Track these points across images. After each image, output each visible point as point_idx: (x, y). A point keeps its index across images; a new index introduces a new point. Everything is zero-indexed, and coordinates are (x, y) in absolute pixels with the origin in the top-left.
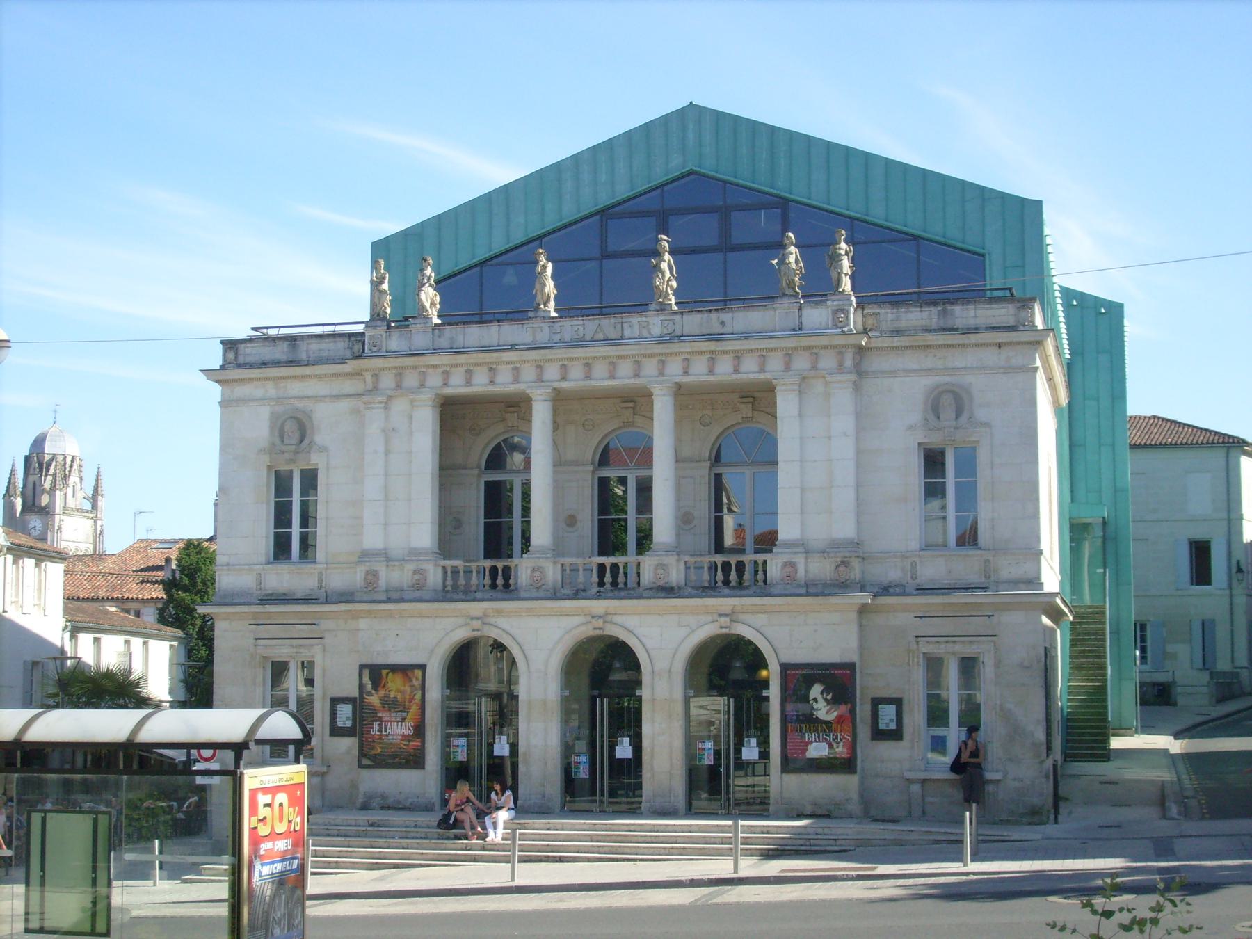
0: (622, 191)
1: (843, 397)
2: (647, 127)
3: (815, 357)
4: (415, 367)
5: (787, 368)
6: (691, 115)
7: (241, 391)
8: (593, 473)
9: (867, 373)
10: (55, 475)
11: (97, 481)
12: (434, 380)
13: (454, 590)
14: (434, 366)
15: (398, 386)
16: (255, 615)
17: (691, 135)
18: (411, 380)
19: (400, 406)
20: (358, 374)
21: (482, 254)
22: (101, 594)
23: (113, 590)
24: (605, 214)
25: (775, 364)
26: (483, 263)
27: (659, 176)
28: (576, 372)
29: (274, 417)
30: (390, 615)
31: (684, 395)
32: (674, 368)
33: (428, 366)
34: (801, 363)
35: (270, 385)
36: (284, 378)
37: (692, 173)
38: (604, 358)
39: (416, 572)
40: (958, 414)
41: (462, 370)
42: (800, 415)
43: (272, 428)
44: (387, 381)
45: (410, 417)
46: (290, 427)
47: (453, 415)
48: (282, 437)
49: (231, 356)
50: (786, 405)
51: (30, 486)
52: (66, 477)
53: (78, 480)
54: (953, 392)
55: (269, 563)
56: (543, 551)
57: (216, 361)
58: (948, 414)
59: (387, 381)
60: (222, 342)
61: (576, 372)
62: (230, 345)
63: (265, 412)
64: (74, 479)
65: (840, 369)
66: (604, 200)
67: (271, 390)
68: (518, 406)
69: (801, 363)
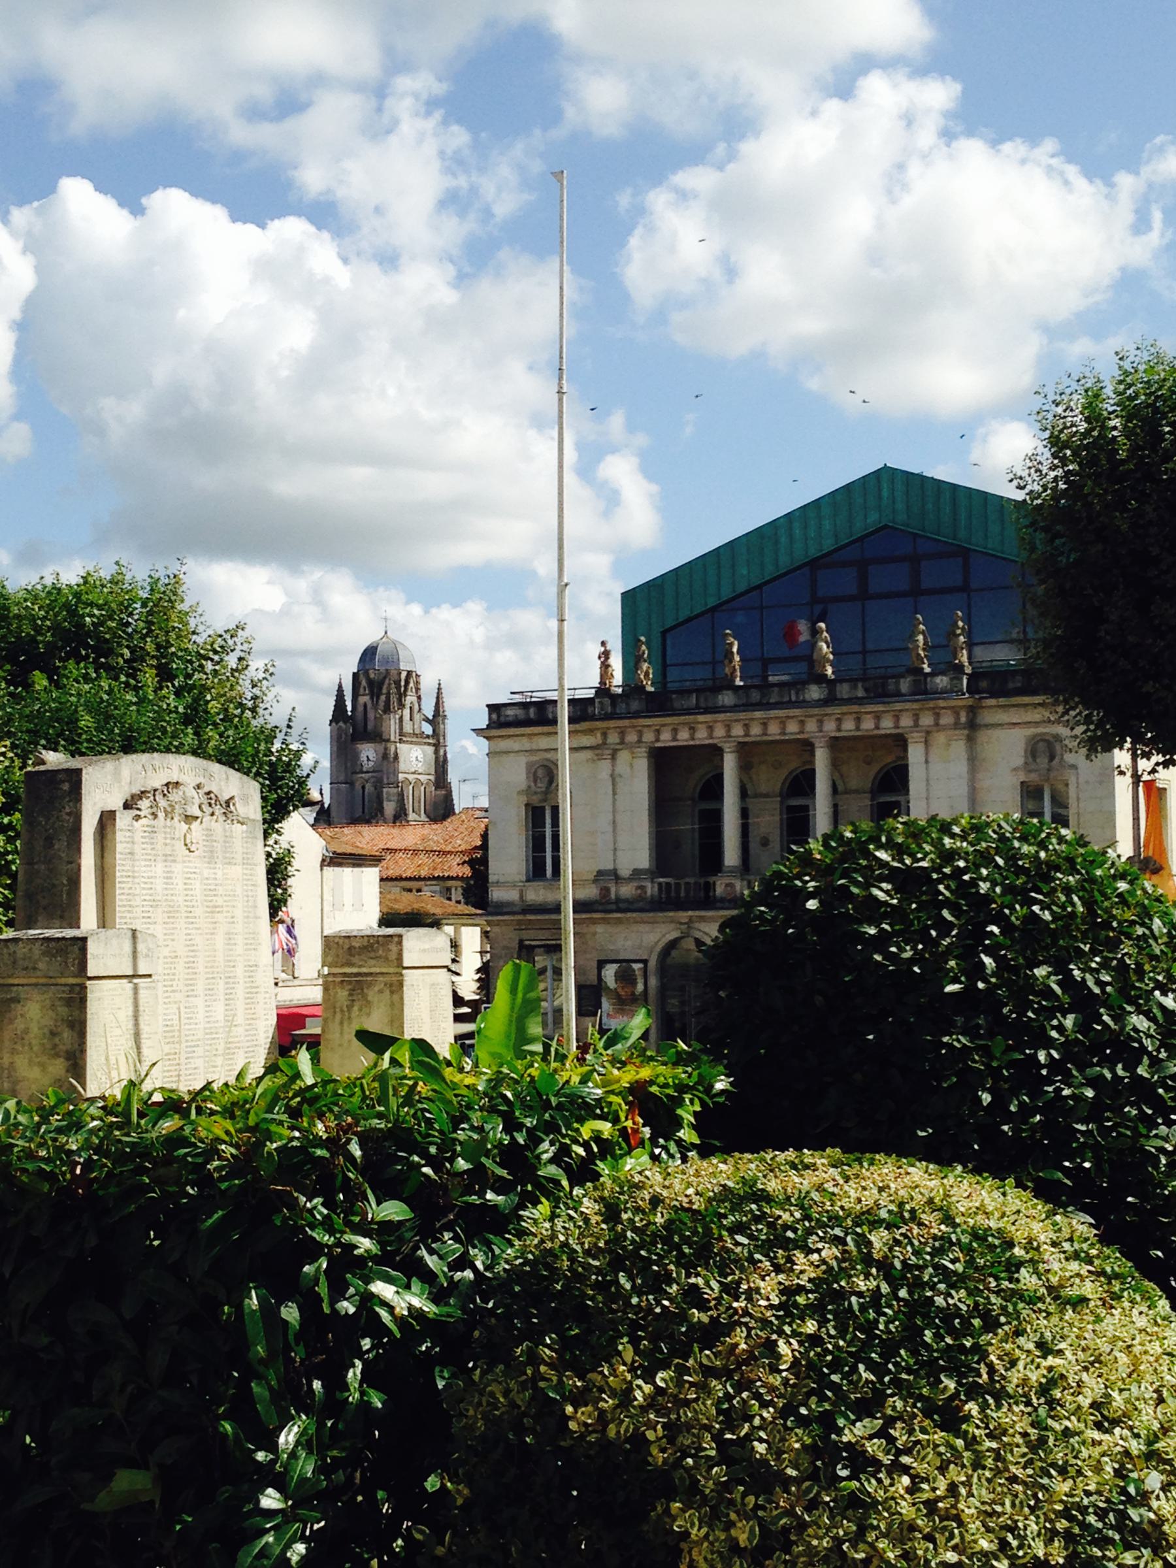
0: (828, 544)
1: (959, 748)
2: (848, 488)
3: (937, 716)
4: (634, 727)
5: (916, 725)
6: (885, 476)
7: (504, 744)
8: (782, 803)
9: (980, 726)
10: (388, 694)
11: (438, 698)
12: (649, 737)
13: (666, 902)
14: (649, 726)
15: (622, 742)
16: (519, 922)
17: (885, 493)
18: (632, 737)
19: (624, 756)
20: (591, 731)
21: (712, 602)
22: (423, 874)
23: (435, 869)
24: (814, 564)
25: (906, 721)
26: (713, 609)
27: (859, 529)
28: (756, 730)
29: (529, 765)
30: (619, 921)
31: (836, 744)
32: (830, 726)
33: (644, 726)
34: (927, 720)
35: (525, 740)
36: (536, 735)
37: (886, 527)
38: (776, 718)
39: (638, 888)
40: (1052, 758)
41: (670, 728)
42: (927, 762)
43: (528, 773)
44: (613, 738)
45: (631, 766)
46: (540, 773)
47: (664, 763)
48: (535, 781)
49: (494, 716)
50: (915, 754)
51: (360, 709)
52: (401, 696)
53: (415, 699)
54: (1042, 740)
55: (528, 880)
56: (732, 870)
57: (484, 723)
58: (1043, 761)
59: (613, 738)
60: (488, 706)
61: (756, 730)
62: (493, 708)
63: (523, 760)
64: (410, 699)
65: (956, 725)
66: (813, 552)
67: (525, 744)
68: (716, 751)
69: (927, 720)
